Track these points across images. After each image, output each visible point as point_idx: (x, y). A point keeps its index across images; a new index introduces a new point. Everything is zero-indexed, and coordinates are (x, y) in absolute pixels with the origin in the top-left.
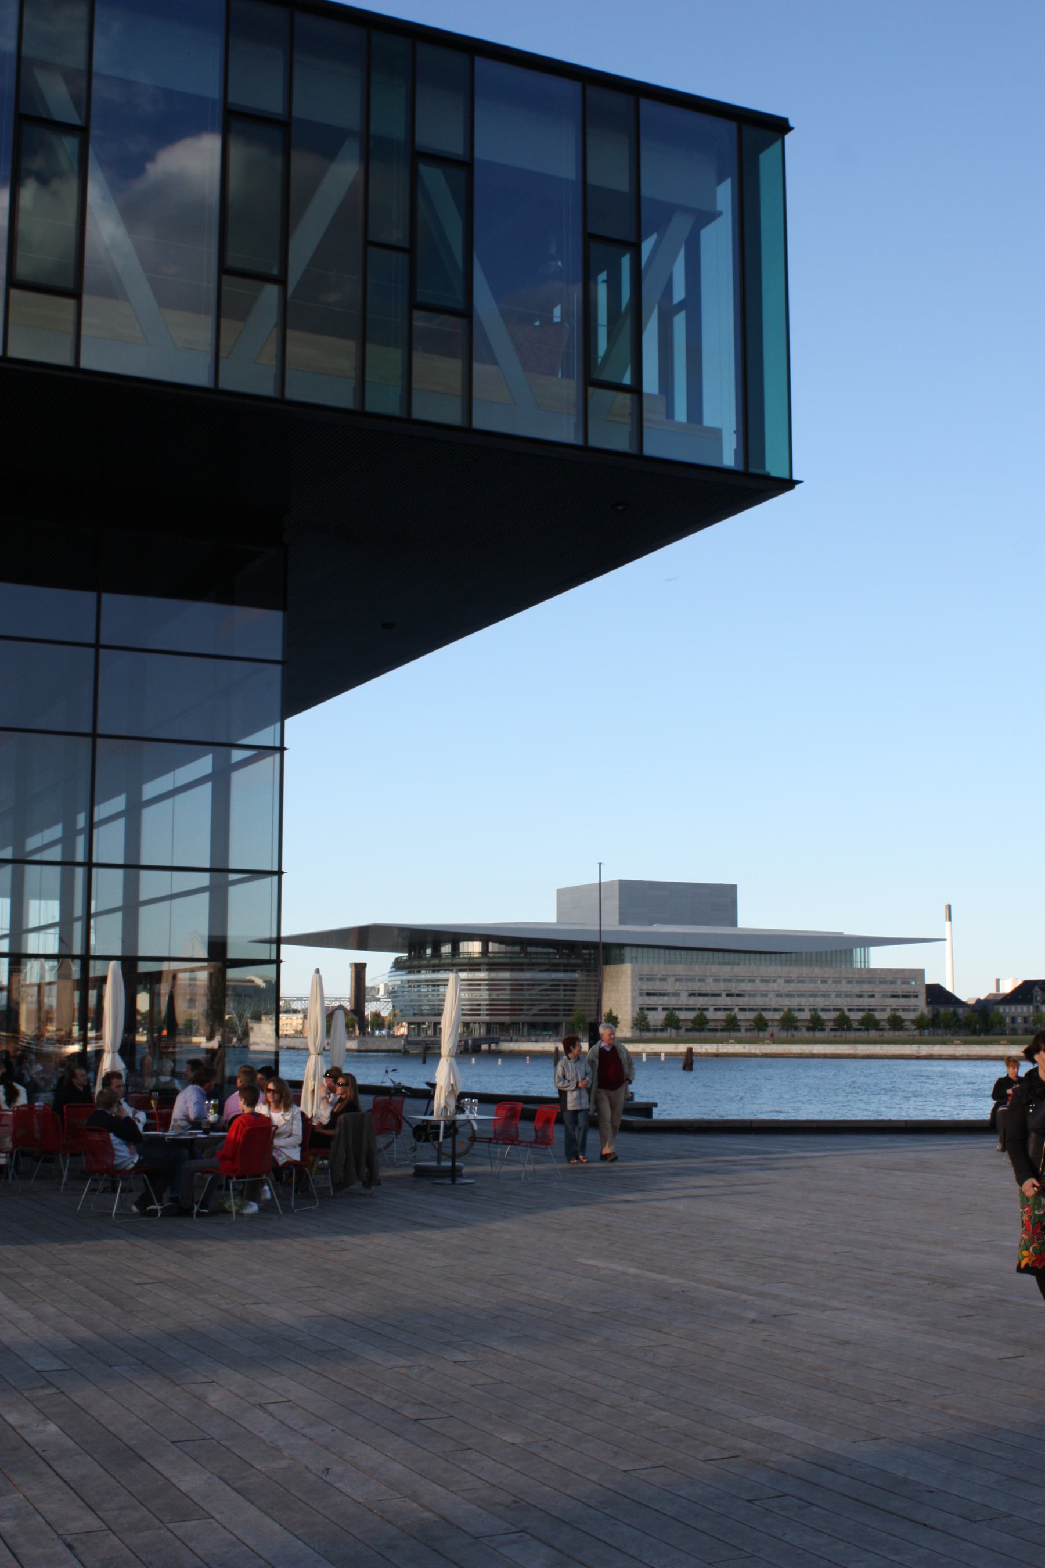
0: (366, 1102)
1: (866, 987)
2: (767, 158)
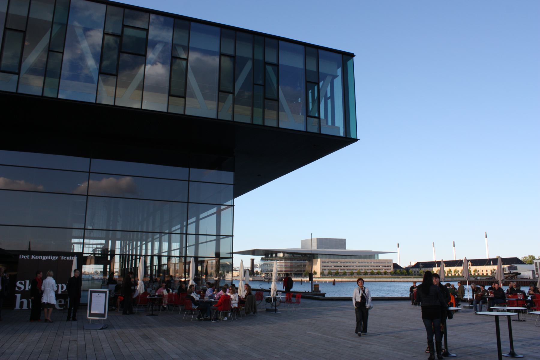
0: (254, 293)
1: (378, 264)
2: (349, 63)
